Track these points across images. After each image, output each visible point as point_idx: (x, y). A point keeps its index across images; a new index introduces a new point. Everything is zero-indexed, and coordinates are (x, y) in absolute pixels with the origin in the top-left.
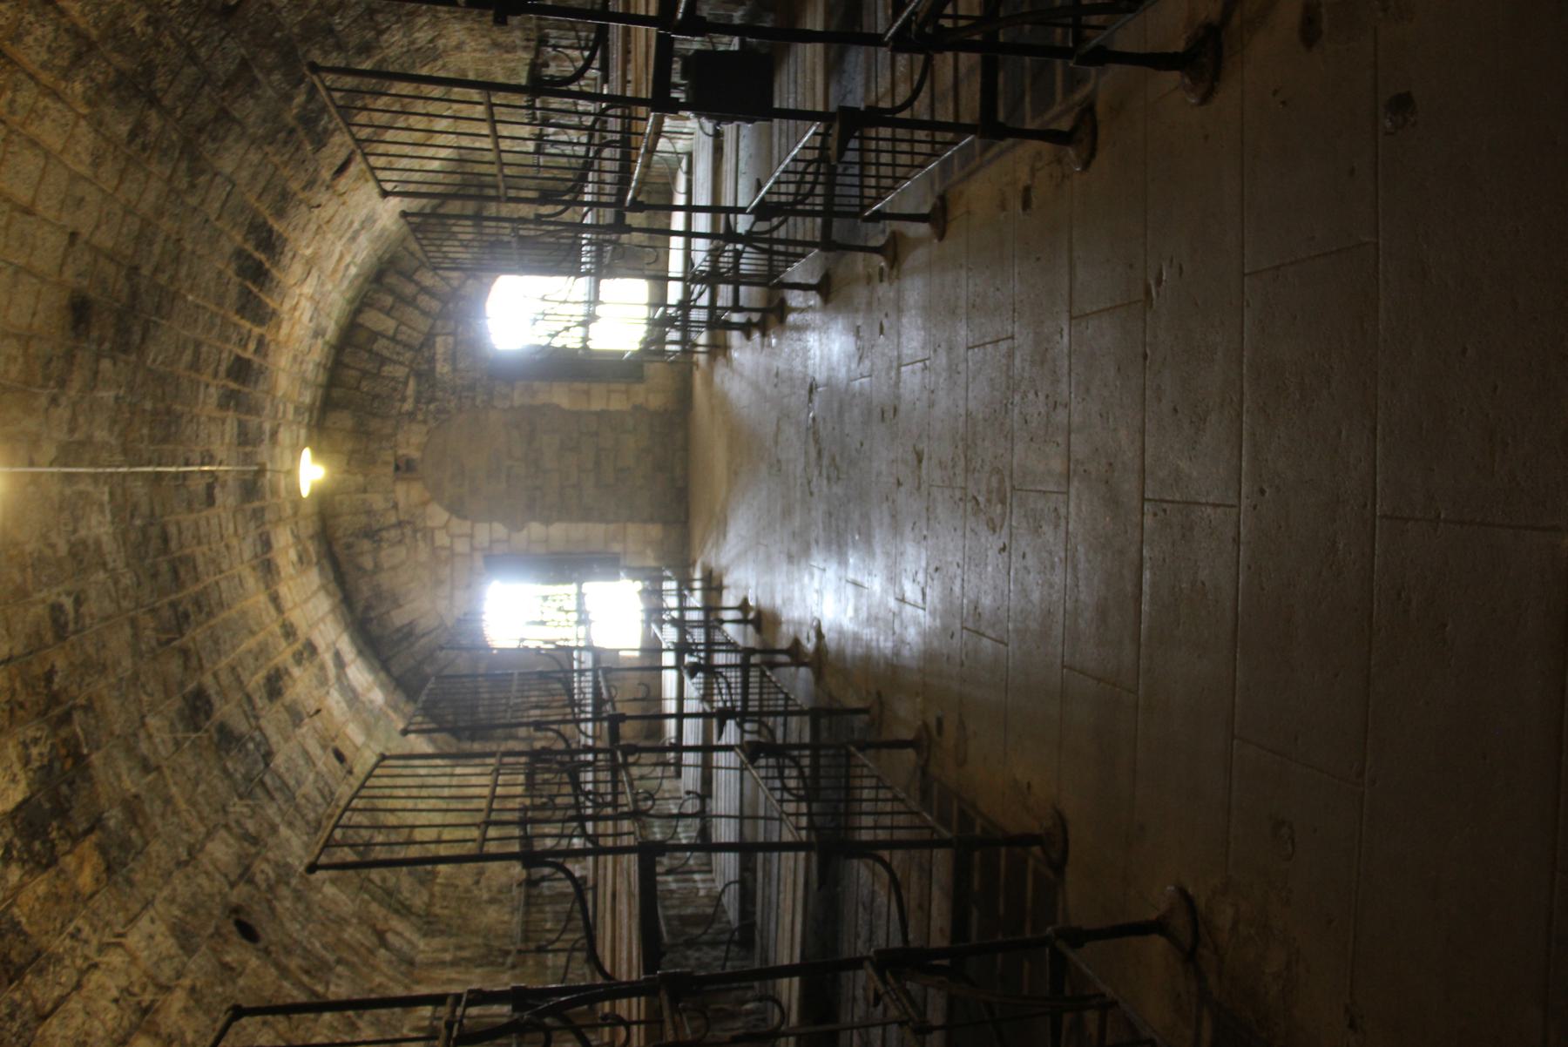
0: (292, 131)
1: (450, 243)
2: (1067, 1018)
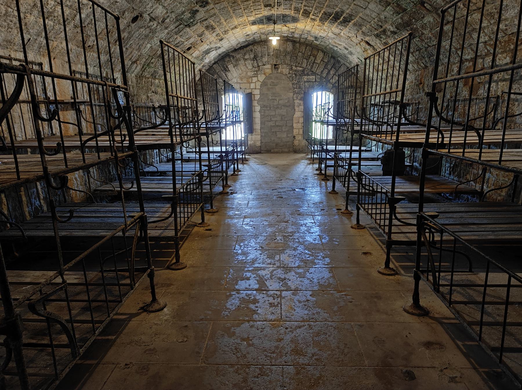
0: (381, 27)
1: (343, 79)
2: (127, 274)
